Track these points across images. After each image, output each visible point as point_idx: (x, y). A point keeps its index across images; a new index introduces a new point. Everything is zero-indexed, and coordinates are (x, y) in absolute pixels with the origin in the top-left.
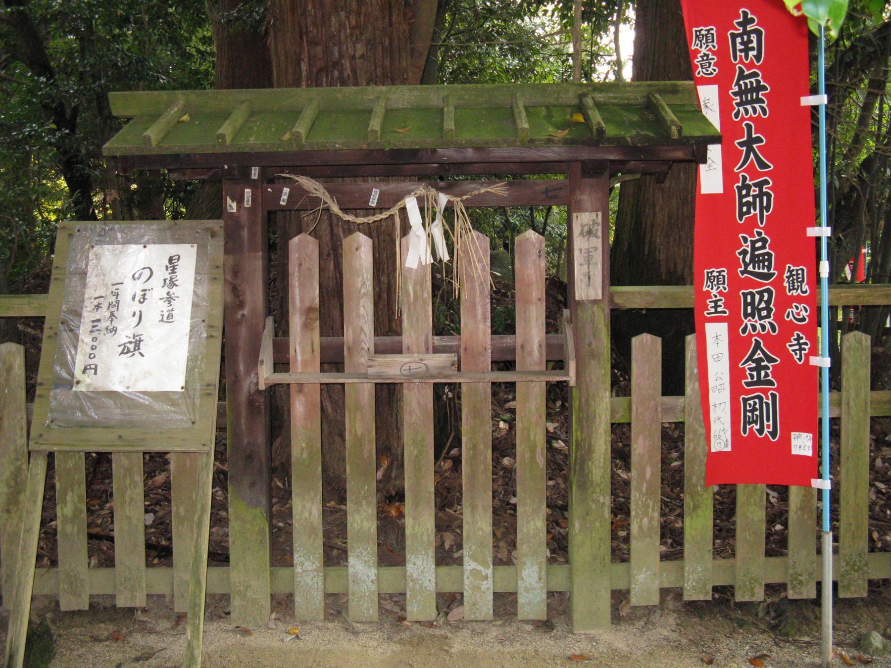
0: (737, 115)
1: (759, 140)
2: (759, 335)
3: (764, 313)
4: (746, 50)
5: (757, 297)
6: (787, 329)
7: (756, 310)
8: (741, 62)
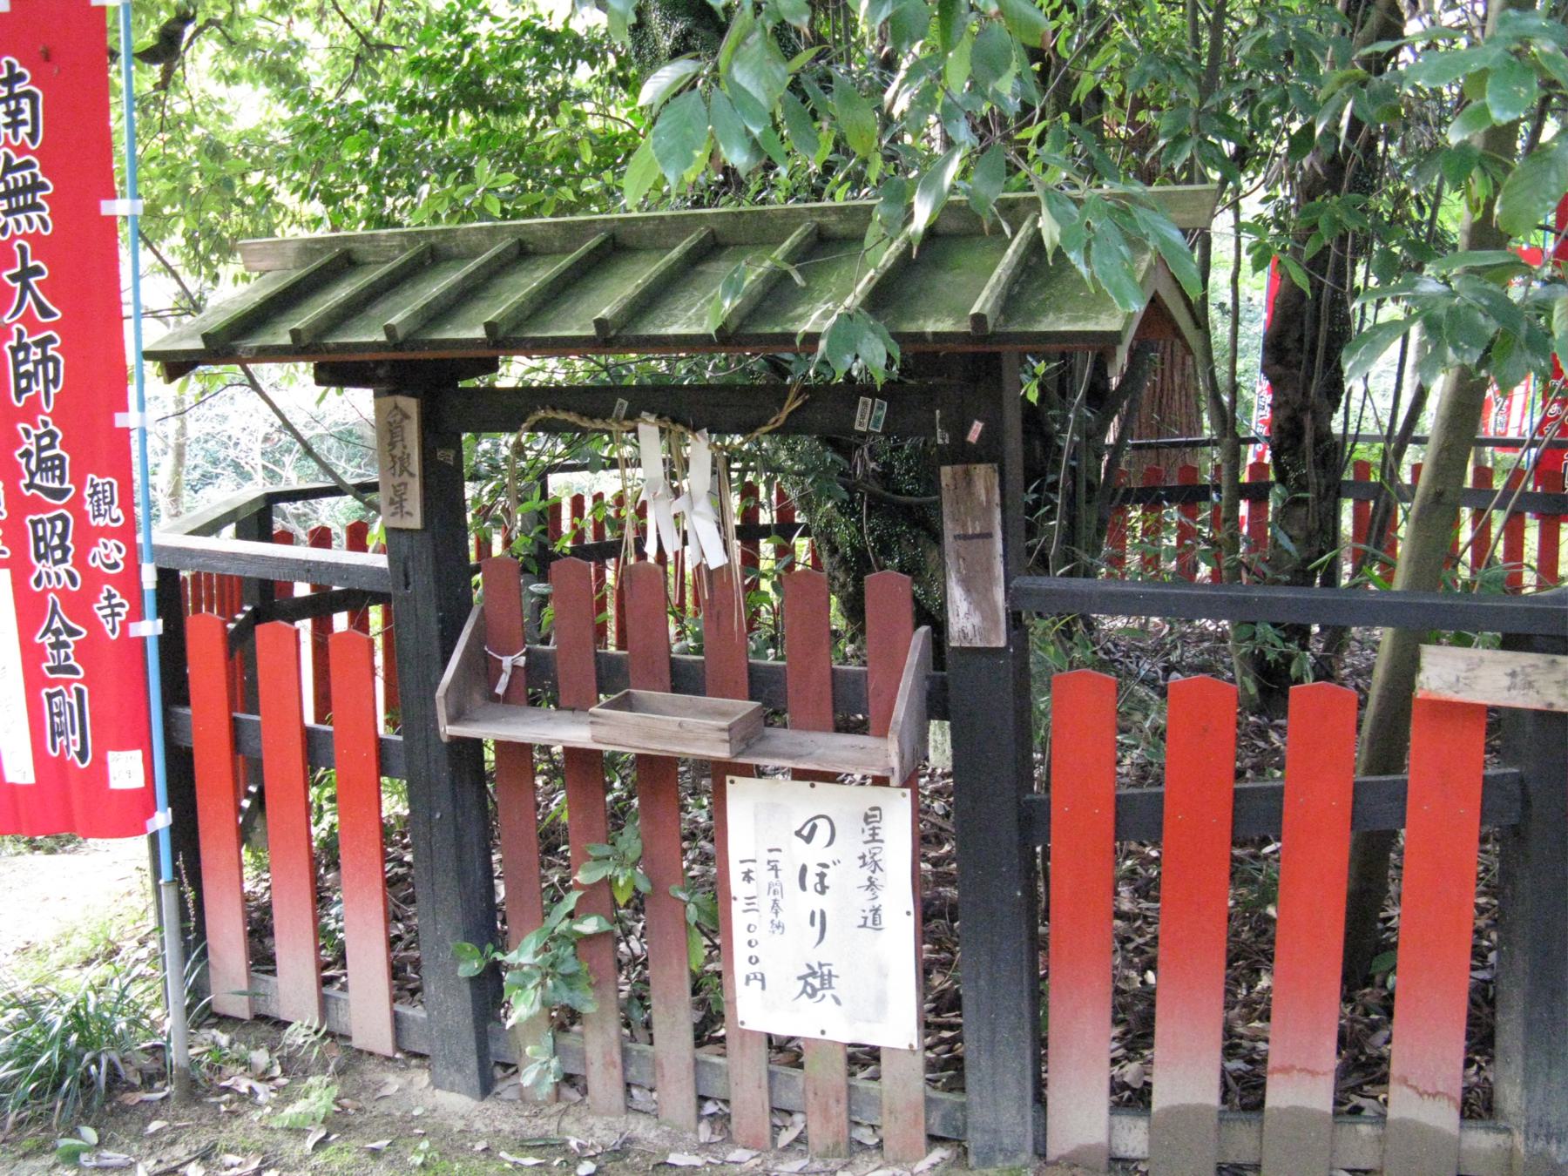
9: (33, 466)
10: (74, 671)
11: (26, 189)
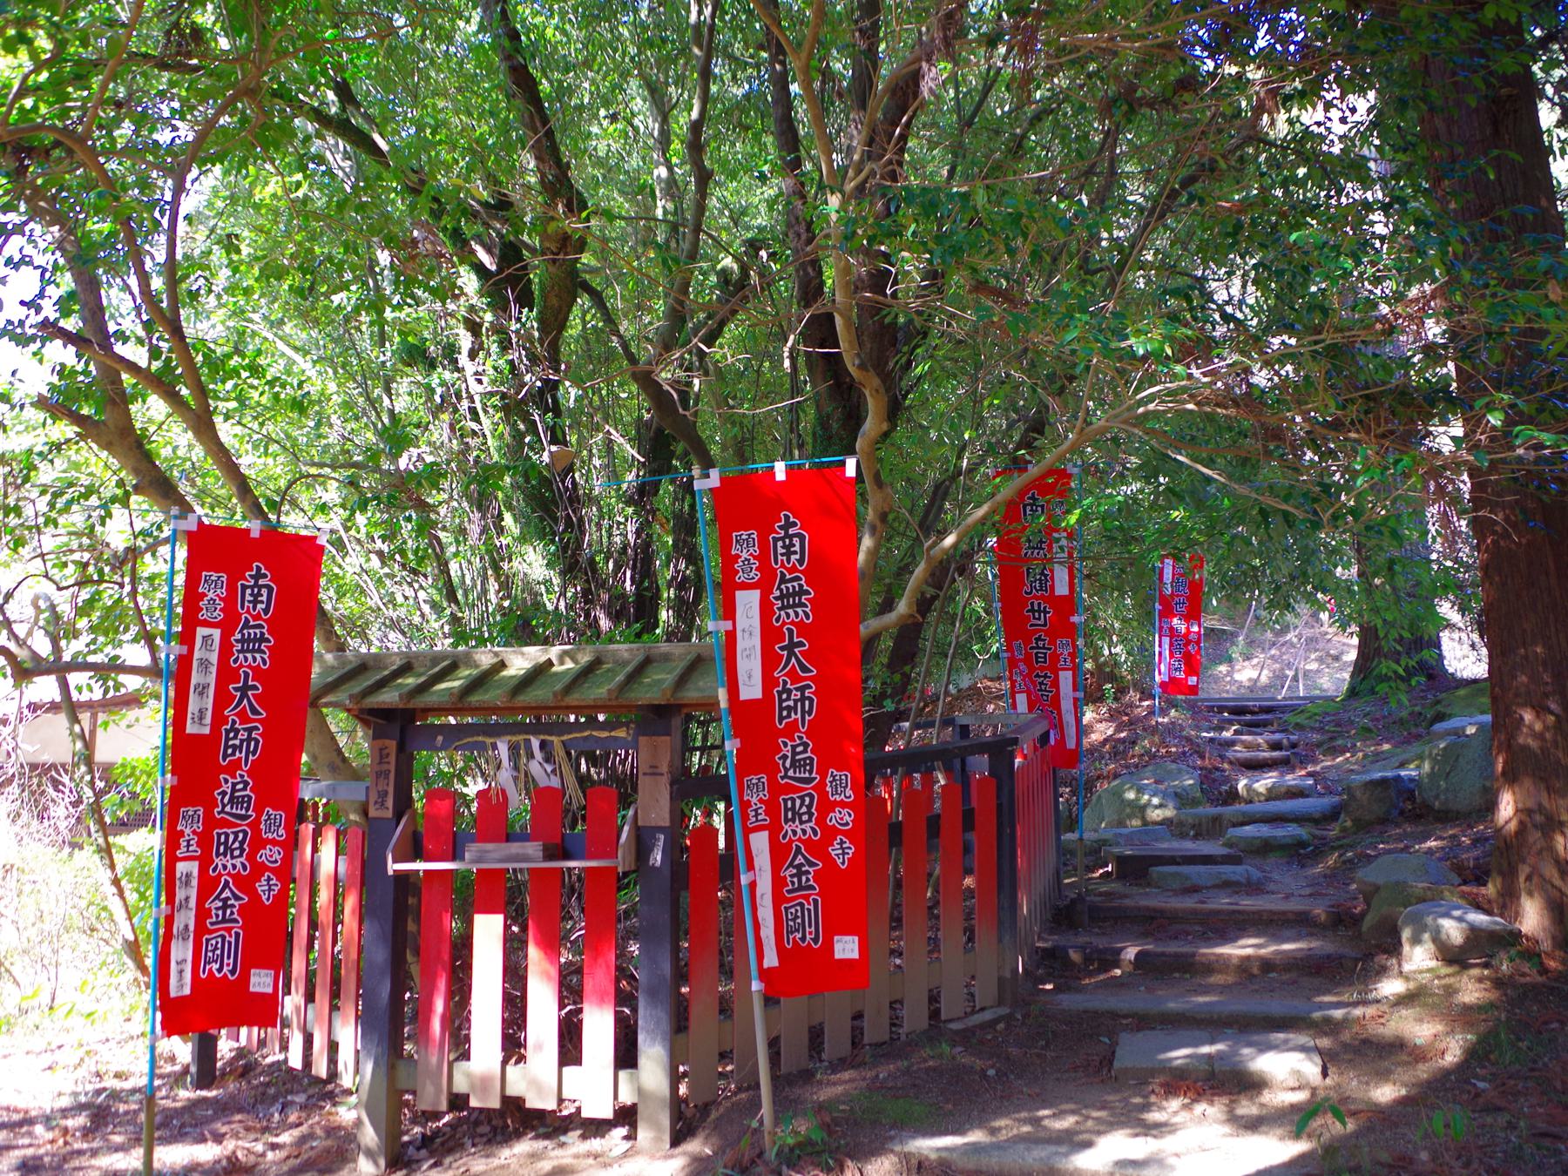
0: (235, 661)
1: (801, 644)
2: (229, 874)
3: (805, 818)
4: (788, 554)
5: (798, 802)
6: (258, 870)
7: (229, 849)
8: (783, 566)
9: (226, 800)
10: (236, 921)
11: (795, 594)
